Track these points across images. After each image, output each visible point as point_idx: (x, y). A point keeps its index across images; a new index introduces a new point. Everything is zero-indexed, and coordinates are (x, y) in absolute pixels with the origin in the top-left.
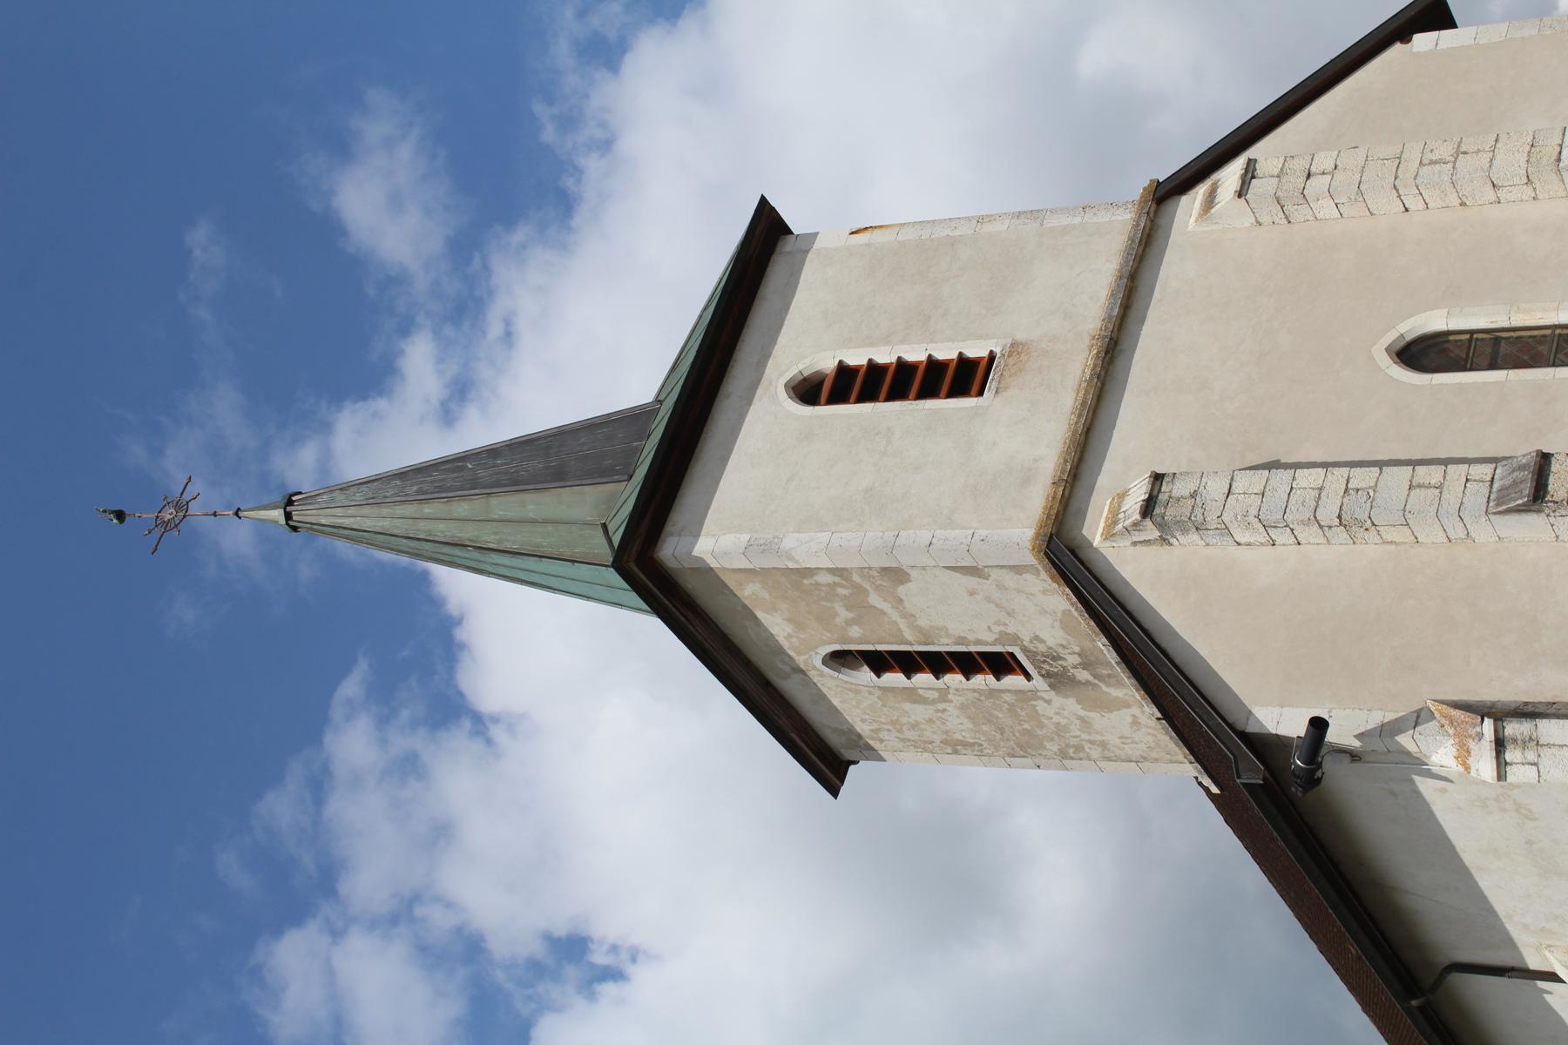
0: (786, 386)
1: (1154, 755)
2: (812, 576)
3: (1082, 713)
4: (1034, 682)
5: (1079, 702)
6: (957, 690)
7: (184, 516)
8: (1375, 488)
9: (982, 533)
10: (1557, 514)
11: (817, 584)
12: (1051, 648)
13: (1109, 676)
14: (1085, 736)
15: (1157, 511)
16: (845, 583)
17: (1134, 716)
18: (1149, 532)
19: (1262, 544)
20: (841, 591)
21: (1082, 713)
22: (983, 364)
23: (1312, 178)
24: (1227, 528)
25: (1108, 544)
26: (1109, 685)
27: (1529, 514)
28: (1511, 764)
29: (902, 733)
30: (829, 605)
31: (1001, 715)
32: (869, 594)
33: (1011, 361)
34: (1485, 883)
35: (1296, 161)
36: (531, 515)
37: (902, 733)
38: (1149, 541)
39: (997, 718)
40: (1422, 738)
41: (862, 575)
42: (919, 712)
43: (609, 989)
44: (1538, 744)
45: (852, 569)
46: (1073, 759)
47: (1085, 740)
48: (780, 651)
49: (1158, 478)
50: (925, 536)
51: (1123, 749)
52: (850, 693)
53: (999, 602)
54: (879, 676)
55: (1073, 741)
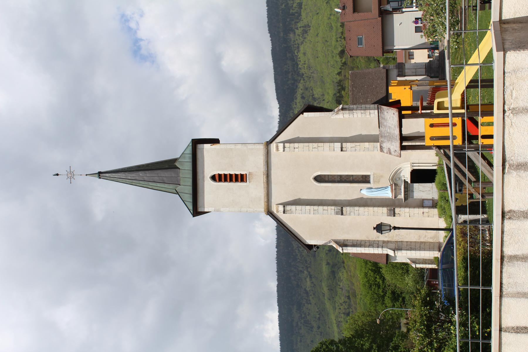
8: (318, 210)
9: (255, 209)
33: (250, 176)
50: (246, 210)
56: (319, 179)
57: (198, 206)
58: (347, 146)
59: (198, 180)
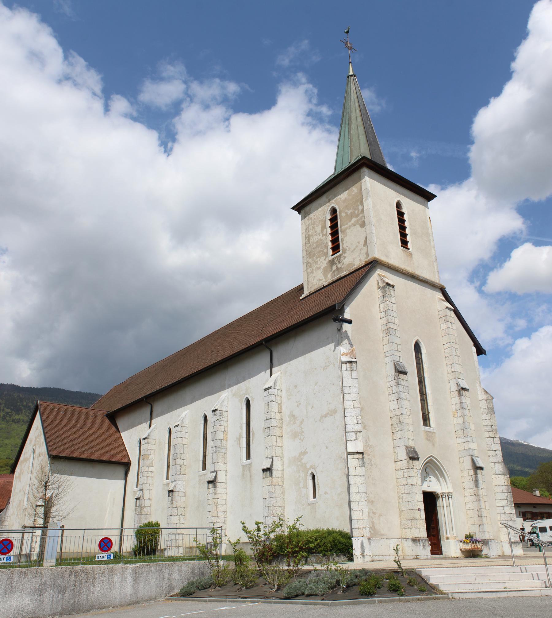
0: (399, 200)
1: (310, 284)
2: (361, 205)
3: (322, 268)
4: (331, 257)
5: (325, 267)
6: (327, 238)
7: (349, 49)
8: (396, 336)
9: (376, 245)
10: (395, 376)
11: (358, 206)
12: (342, 261)
13: (335, 274)
14: (314, 268)
15: (387, 286)
16: (359, 212)
17: (322, 280)
18: (382, 284)
19: (380, 310)
20: (356, 212)
21: (322, 268)
22: (407, 247)
23: (450, 323)
24: (384, 302)
25: (377, 275)
26: (332, 274)
27: (395, 370)
28: (346, 365)
29: (311, 225)
30: (352, 208)
31: (319, 249)
32: (356, 218)
33: (409, 254)
34: (300, 359)
35: (453, 320)
36: (360, 137)
37: (311, 225)
38: (379, 284)
39: (318, 248)
40: (347, 345)
41: (362, 217)
42: (318, 229)
43: (162, 149)
44: (351, 371)
45: (364, 214)
46: (307, 265)
47: (313, 268)
48: (335, 196)
49: (393, 286)
50: (374, 232)
51: (311, 277)
52: (323, 213)
53: (356, 249)
54: (329, 220)
55: (312, 265)
56: (417, 347)
57: (370, 170)
58: (467, 398)
59: (396, 184)
